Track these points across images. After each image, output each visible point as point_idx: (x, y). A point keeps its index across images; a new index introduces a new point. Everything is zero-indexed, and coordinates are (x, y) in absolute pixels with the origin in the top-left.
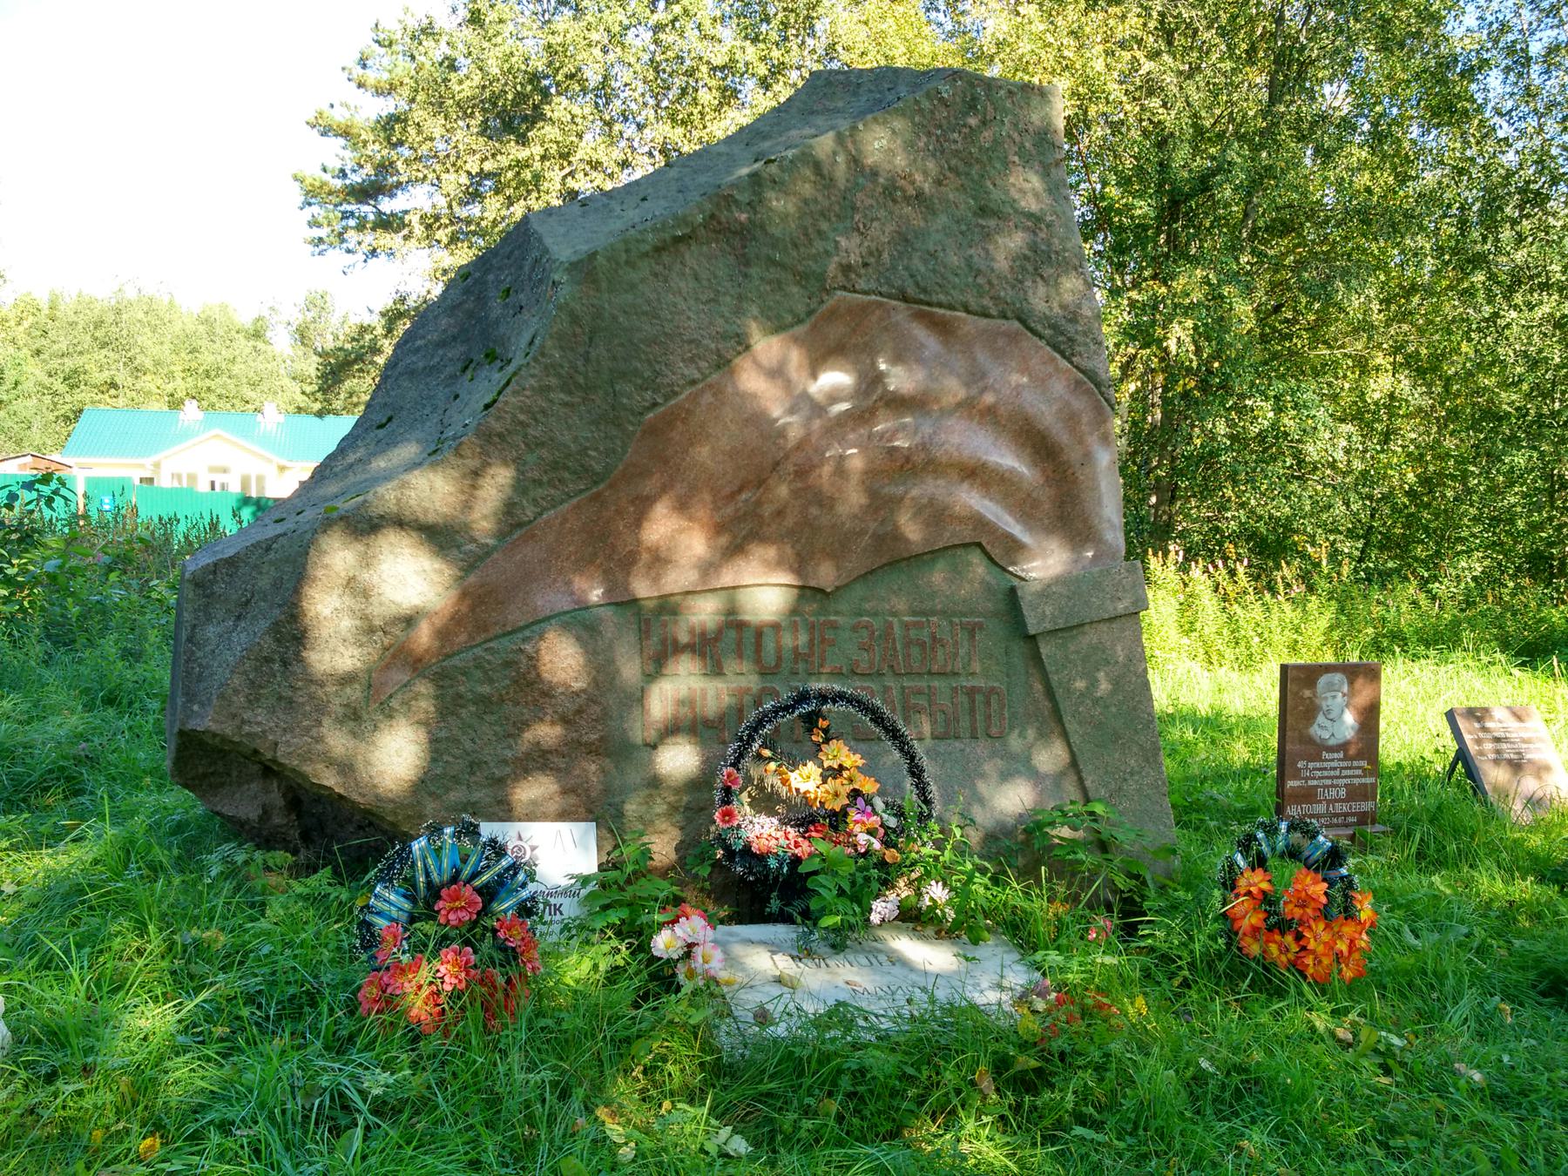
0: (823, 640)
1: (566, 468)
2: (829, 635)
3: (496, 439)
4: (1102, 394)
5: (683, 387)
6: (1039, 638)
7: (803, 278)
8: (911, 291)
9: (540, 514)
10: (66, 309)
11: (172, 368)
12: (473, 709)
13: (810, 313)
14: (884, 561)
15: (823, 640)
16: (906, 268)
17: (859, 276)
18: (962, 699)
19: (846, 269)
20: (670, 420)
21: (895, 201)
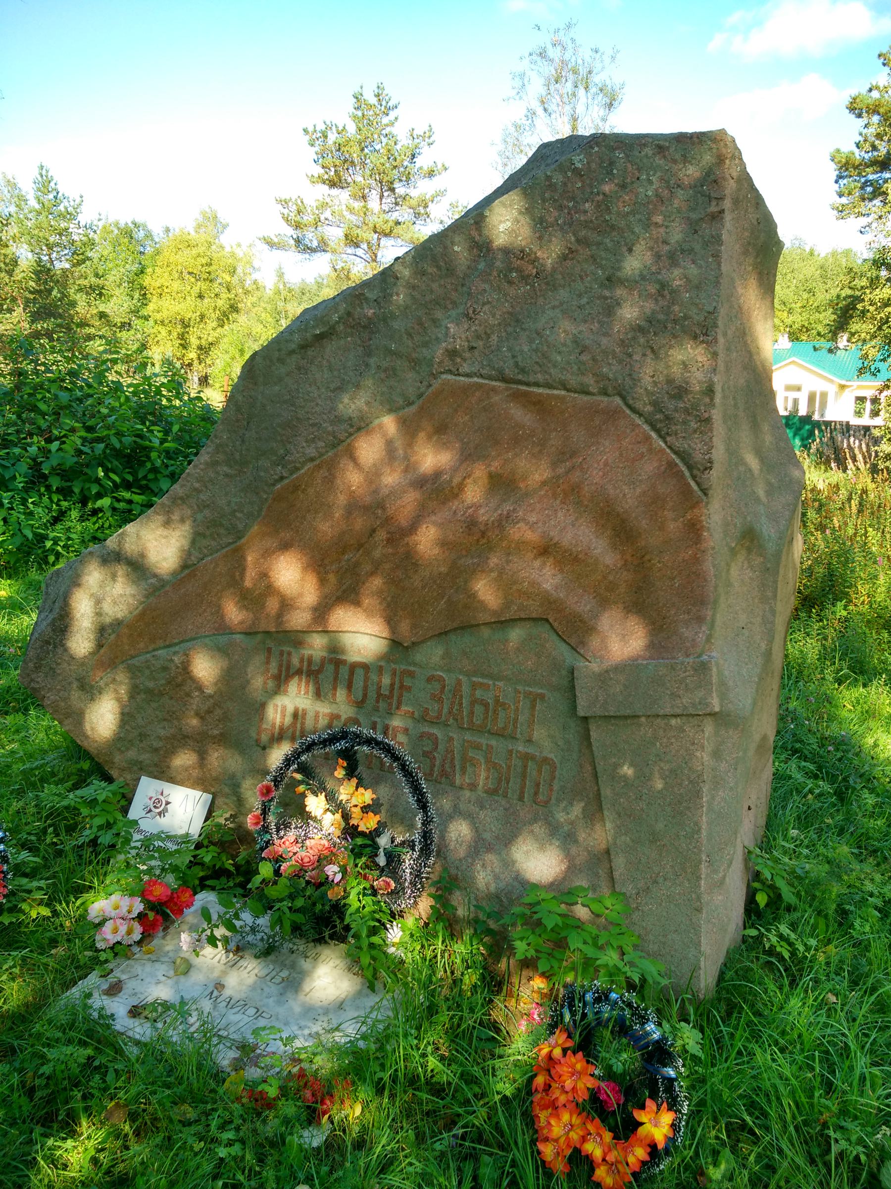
0: (402, 687)
1: (221, 525)
2: (407, 682)
3: (179, 502)
4: (694, 477)
5: (304, 464)
6: (591, 721)
7: (415, 363)
8: (509, 372)
9: (202, 559)
10: (839, 251)
11: (793, 305)
12: (144, 696)
13: (420, 396)
14: (455, 625)
15: (402, 687)
16: (510, 349)
17: (465, 360)
18: (516, 762)
19: (452, 354)
20: (295, 488)
21: (511, 283)
